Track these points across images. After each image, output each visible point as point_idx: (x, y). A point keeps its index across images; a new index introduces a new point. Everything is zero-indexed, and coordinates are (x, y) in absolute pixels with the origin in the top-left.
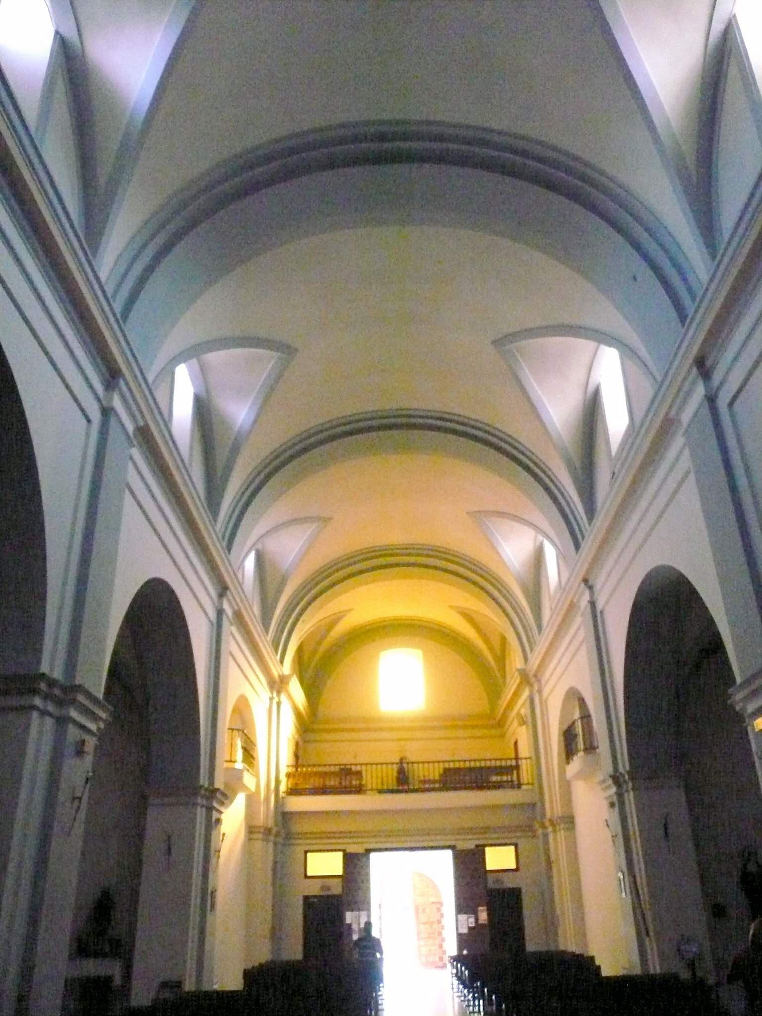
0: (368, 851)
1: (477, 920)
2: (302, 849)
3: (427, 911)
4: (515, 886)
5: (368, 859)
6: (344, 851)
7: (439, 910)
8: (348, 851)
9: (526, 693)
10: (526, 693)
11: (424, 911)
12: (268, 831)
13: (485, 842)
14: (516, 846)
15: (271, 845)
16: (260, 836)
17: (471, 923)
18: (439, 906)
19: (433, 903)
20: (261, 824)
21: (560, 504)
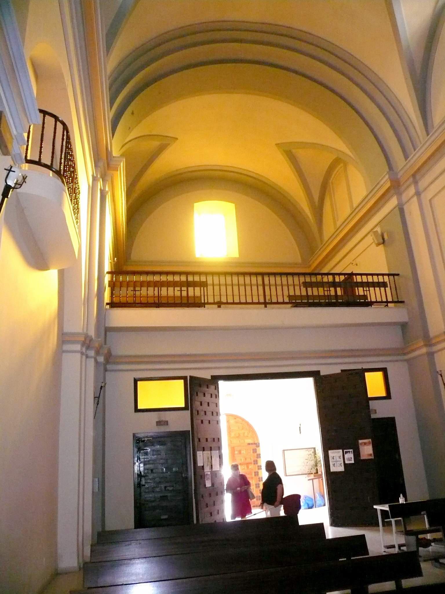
0: (215, 379)
1: (357, 454)
2: (129, 378)
3: (243, 452)
4: (156, 423)
5: (217, 388)
6: (184, 378)
7: (255, 451)
8: (325, 371)
9: (393, 202)
10: (393, 202)
11: (240, 452)
12: (87, 343)
13: (365, 367)
14: (384, 371)
15: (91, 363)
16: (78, 347)
17: (350, 459)
18: (254, 447)
19: (249, 444)
20: (80, 331)
21: (22, 100)
